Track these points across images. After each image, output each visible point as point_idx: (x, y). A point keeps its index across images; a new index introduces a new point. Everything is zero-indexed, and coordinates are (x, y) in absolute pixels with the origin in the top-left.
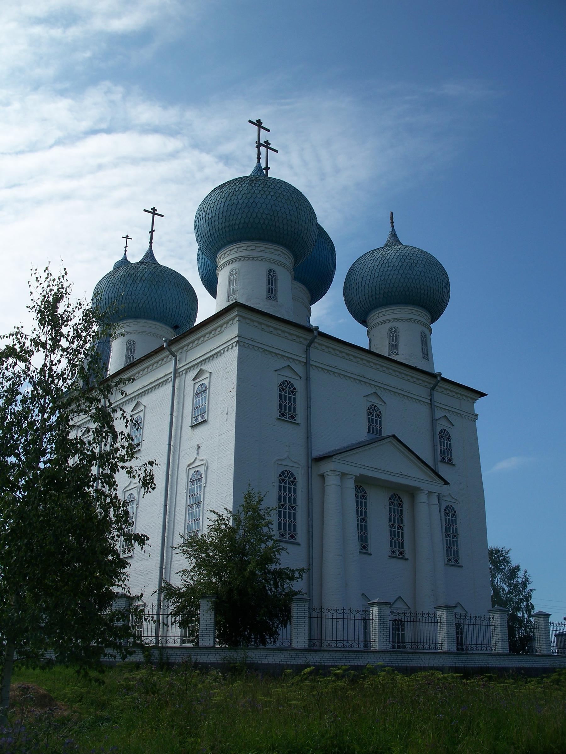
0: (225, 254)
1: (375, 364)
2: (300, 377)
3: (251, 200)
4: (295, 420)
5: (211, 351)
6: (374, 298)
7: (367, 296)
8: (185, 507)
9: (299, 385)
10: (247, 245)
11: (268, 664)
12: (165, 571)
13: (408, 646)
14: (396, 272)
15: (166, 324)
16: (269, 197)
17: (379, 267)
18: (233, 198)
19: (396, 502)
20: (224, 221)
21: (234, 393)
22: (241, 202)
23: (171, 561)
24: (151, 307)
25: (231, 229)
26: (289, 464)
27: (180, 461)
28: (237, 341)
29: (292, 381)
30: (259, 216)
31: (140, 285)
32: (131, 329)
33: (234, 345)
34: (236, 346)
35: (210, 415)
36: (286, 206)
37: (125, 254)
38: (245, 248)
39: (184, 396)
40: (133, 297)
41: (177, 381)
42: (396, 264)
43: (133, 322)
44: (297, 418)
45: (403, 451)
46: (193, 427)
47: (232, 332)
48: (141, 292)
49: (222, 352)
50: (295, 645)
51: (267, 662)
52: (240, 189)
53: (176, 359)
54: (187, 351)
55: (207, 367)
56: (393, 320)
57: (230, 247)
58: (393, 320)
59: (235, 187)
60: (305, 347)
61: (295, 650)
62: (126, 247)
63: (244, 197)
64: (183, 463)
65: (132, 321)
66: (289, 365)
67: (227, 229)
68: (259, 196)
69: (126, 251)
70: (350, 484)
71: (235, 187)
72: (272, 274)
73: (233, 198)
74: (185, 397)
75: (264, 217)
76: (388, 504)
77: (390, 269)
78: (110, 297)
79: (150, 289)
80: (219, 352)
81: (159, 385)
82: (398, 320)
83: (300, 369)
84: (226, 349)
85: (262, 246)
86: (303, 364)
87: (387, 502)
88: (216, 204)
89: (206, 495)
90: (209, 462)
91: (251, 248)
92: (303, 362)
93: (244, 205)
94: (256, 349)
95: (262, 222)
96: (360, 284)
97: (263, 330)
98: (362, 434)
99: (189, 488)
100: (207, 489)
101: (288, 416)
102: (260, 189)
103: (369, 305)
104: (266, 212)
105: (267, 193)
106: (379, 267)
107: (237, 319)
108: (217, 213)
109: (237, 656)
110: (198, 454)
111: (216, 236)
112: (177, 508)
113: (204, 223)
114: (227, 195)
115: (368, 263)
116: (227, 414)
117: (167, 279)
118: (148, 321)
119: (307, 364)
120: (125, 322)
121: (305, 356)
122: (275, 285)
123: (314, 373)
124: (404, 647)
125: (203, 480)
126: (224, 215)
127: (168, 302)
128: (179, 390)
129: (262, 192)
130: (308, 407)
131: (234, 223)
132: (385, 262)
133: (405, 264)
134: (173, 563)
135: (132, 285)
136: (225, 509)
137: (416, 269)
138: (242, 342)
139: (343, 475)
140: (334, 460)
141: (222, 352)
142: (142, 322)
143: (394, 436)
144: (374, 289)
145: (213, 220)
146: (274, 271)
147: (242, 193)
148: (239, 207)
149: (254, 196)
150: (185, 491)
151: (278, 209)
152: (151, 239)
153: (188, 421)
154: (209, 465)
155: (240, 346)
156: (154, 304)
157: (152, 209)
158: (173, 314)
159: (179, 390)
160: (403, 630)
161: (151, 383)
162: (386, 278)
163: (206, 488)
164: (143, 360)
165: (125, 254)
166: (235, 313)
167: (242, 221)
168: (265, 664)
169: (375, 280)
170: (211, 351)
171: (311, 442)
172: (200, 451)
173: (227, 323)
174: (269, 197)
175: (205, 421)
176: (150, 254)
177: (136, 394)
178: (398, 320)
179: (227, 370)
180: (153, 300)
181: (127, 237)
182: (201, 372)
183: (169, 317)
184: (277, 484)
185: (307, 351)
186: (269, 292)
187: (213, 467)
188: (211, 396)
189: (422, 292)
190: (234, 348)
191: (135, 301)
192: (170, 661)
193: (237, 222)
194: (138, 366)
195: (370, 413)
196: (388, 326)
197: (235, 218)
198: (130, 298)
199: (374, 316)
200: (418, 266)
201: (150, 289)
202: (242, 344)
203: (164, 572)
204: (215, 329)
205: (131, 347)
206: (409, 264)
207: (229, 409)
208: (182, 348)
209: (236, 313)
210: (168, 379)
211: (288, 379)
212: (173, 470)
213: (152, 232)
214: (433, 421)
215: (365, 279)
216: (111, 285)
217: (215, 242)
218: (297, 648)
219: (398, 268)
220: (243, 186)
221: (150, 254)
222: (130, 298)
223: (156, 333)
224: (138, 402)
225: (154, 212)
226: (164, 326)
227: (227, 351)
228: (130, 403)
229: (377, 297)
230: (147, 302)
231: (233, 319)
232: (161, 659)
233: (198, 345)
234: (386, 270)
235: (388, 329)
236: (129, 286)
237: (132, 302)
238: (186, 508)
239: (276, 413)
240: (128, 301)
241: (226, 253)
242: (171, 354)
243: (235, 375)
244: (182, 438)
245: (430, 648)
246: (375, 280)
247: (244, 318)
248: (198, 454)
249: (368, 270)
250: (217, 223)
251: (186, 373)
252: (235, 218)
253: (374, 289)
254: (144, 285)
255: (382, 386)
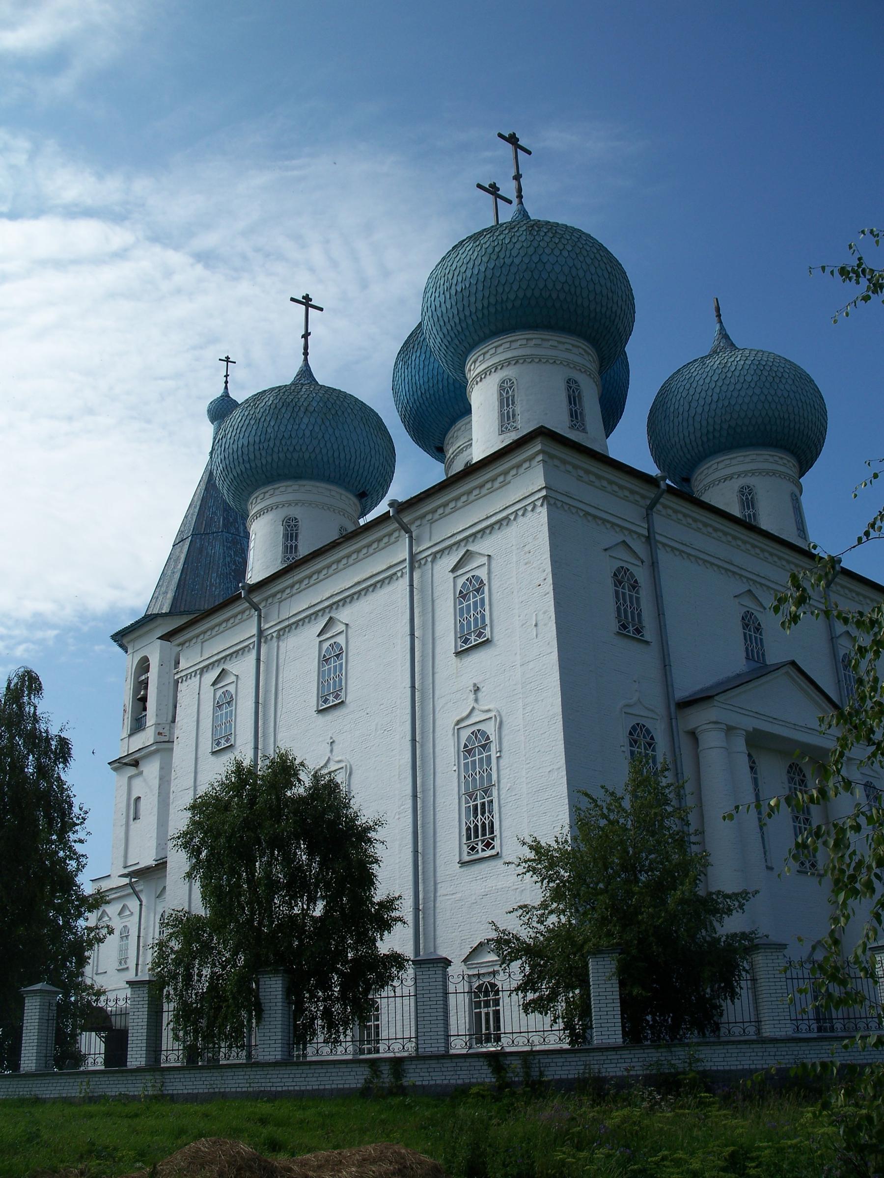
0: (484, 354)
1: (745, 542)
2: (642, 562)
3: (535, 259)
4: (642, 636)
5: (487, 518)
6: (711, 436)
7: (698, 435)
8: (457, 797)
9: (641, 574)
10: (527, 336)
11: (730, 1070)
12: (424, 913)
13: (838, 1025)
14: (750, 393)
15: (347, 489)
16: (565, 253)
17: (720, 383)
18: (502, 255)
19: (797, 778)
20: (487, 295)
21: (548, 587)
22: (517, 261)
23: (435, 897)
24: (325, 459)
25: (499, 309)
26: (642, 713)
27: (437, 716)
28: (545, 497)
29: (632, 569)
30: (550, 286)
31: (306, 420)
32: (290, 497)
33: (539, 503)
34: (542, 505)
35: (495, 631)
36: (593, 270)
37: (226, 388)
38: (524, 342)
39: (433, 601)
40: (294, 442)
41: (416, 575)
42: (749, 378)
43: (293, 485)
44: (644, 633)
45: (805, 686)
46: (458, 654)
47: (531, 480)
48: (307, 433)
49: (512, 518)
50: (768, 1031)
51: (727, 1068)
52: (514, 240)
53: (411, 537)
54: (432, 522)
55: (481, 547)
56: (745, 473)
57: (482, 349)
58: (745, 473)
59: (502, 237)
60: (644, 511)
61: (774, 1041)
62: (227, 376)
63: (522, 253)
64: (457, 718)
65: (289, 483)
66: (624, 542)
67: (492, 310)
68: (548, 251)
69: (226, 382)
70: (740, 745)
71: (502, 237)
72: (573, 386)
73: (502, 255)
74: (436, 603)
75: (559, 287)
76: (786, 781)
77: (738, 386)
78: (251, 441)
79: (323, 427)
80: (507, 518)
81: (374, 585)
82: (760, 473)
83: (639, 547)
84: (520, 513)
85: (553, 338)
86: (643, 540)
87: (785, 778)
88: (471, 265)
89: (502, 773)
90: (503, 714)
91: (534, 342)
92: (643, 535)
93: (524, 267)
94: (574, 511)
95: (554, 296)
96: (686, 414)
97: (579, 478)
98: (738, 663)
99: (462, 762)
100: (502, 762)
101: (631, 629)
102: (547, 239)
103: (701, 449)
104: (562, 279)
105: (561, 246)
106: (720, 383)
107: (540, 457)
108: (473, 281)
109: (676, 1059)
110: (476, 700)
111: (470, 322)
112: (438, 801)
113: (448, 301)
114: (490, 250)
115: (697, 379)
116: (536, 625)
117: (349, 411)
118: (318, 484)
119: (649, 539)
120: (276, 486)
121: (646, 526)
122: (581, 406)
123: (663, 556)
124: (832, 1029)
125: (494, 747)
126: (487, 284)
127: (353, 450)
128: (422, 591)
129: (552, 245)
130: (660, 613)
131: (505, 298)
132: (729, 375)
133: (763, 379)
134: (439, 899)
135: (292, 421)
136: (602, 787)
137: (781, 386)
138: (553, 499)
139: (730, 730)
140: (715, 703)
141: (512, 518)
142: (308, 485)
143: (793, 663)
144: (711, 421)
145: (466, 293)
146: (576, 382)
147: (518, 246)
148: (514, 269)
149: (540, 251)
150: (455, 768)
151: (581, 273)
152: (306, 347)
153: (447, 642)
154: (504, 719)
155: (549, 504)
156: (330, 453)
157: (303, 297)
158: (361, 471)
159: (422, 591)
160: (497, 1003)
161: (359, 583)
162: (733, 402)
163: (501, 761)
164: (339, 544)
165: (226, 388)
166: (537, 446)
167: (521, 295)
168: (724, 1071)
169: (713, 406)
170: (487, 518)
171: (671, 675)
172: (480, 694)
173: (518, 466)
174: (565, 253)
175: (488, 642)
176: (306, 372)
177: (326, 604)
178: (753, 474)
179: (527, 549)
180: (329, 445)
181: (227, 360)
182: (468, 556)
183: (354, 476)
184: (627, 749)
185: (648, 517)
186: (572, 416)
187: (514, 722)
188: (495, 597)
189: (792, 426)
190: (539, 509)
191: (298, 448)
192: (545, 1079)
193: (512, 296)
194: (328, 554)
195: (746, 626)
196: (742, 481)
197: (507, 290)
198: (288, 443)
199: (708, 468)
200: (784, 381)
201: (323, 427)
202: (552, 501)
203: (421, 917)
204: (493, 480)
205: (291, 531)
206: (770, 379)
207: (541, 617)
208: (423, 517)
209: (539, 447)
210: (395, 574)
211: (625, 565)
212: (423, 733)
213: (306, 335)
214: (832, 639)
215: (694, 404)
216: (252, 422)
217: (467, 334)
218: (779, 1037)
219: (753, 385)
220: (518, 234)
221: (306, 372)
222: (288, 443)
223: (321, 511)
224: (331, 618)
225: (307, 302)
226: (344, 492)
227: (523, 515)
228: (313, 622)
229: (717, 434)
230: (317, 451)
231: (531, 459)
232: (527, 1074)
233: (455, 510)
234: (731, 388)
235: (737, 488)
236: (285, 421)
237: (291, 449)
238: (459, 799)
239: (614, 626)
240: (285, 449)
241: (487, 352)
242: (403, 528)
243: (547, 555)
244: (437, 676)
245: (810, 1030)
246: (713, 406)
247: (552, 457)
248: (476, 700)
249: (698, 390)
250: (473, 299)
251: (433, 561)
252: (507, 290)
253: (711, 421)
254: (313, 420)
255: (758, 579)
